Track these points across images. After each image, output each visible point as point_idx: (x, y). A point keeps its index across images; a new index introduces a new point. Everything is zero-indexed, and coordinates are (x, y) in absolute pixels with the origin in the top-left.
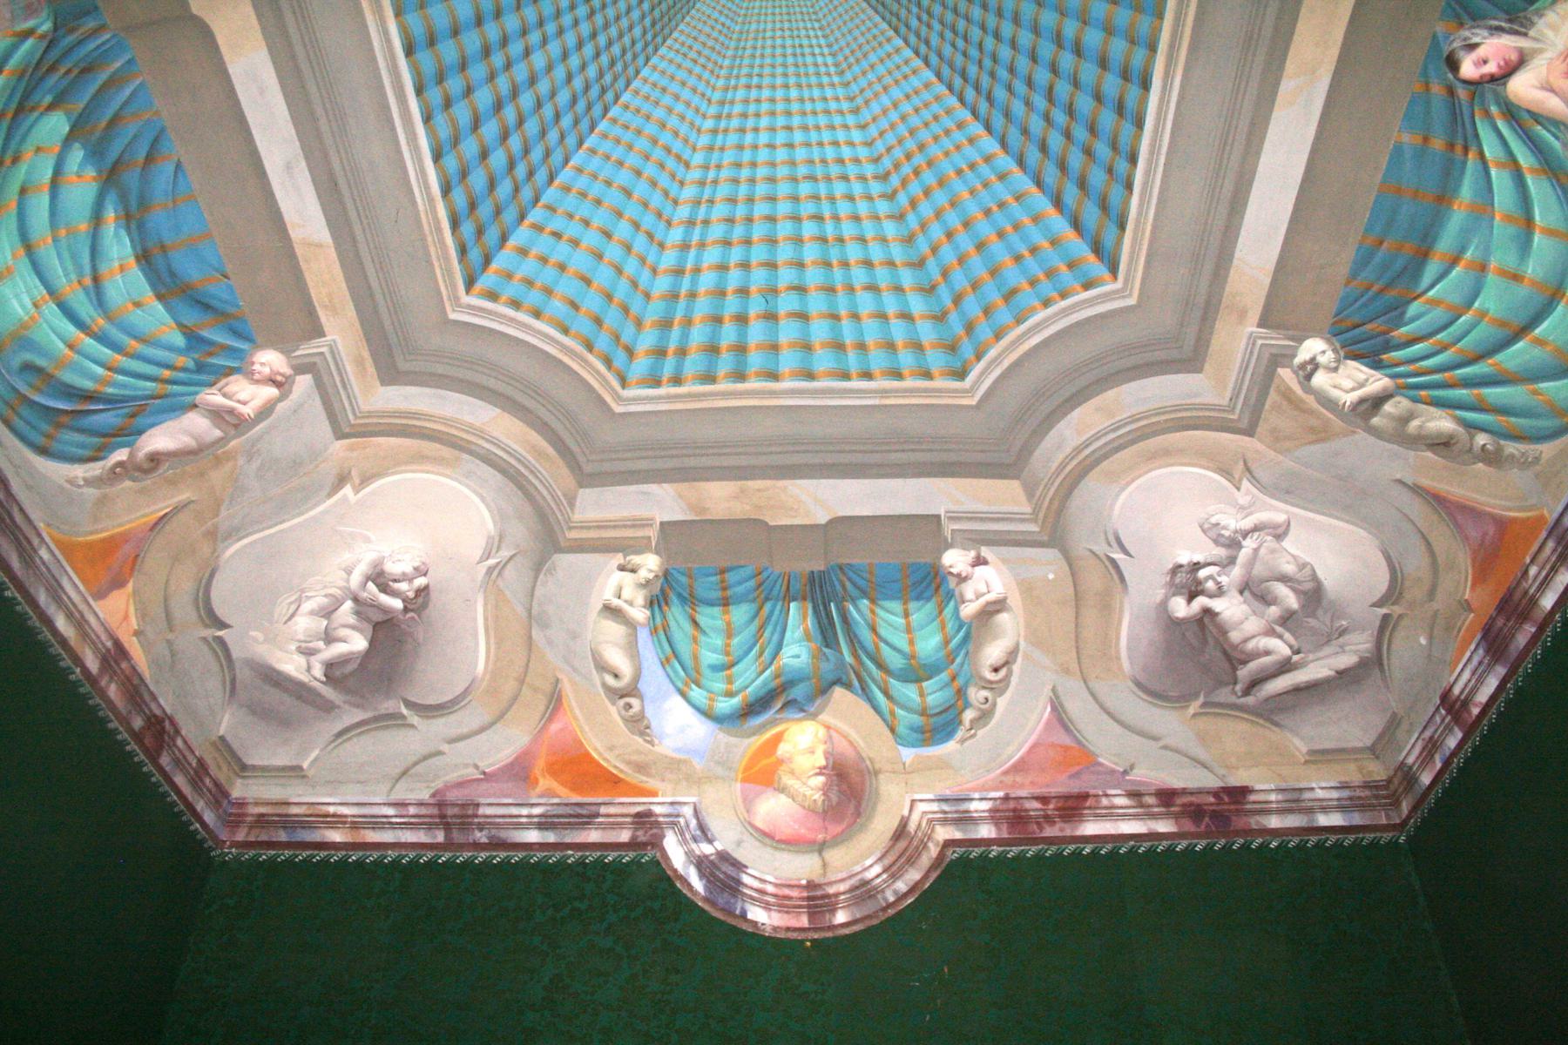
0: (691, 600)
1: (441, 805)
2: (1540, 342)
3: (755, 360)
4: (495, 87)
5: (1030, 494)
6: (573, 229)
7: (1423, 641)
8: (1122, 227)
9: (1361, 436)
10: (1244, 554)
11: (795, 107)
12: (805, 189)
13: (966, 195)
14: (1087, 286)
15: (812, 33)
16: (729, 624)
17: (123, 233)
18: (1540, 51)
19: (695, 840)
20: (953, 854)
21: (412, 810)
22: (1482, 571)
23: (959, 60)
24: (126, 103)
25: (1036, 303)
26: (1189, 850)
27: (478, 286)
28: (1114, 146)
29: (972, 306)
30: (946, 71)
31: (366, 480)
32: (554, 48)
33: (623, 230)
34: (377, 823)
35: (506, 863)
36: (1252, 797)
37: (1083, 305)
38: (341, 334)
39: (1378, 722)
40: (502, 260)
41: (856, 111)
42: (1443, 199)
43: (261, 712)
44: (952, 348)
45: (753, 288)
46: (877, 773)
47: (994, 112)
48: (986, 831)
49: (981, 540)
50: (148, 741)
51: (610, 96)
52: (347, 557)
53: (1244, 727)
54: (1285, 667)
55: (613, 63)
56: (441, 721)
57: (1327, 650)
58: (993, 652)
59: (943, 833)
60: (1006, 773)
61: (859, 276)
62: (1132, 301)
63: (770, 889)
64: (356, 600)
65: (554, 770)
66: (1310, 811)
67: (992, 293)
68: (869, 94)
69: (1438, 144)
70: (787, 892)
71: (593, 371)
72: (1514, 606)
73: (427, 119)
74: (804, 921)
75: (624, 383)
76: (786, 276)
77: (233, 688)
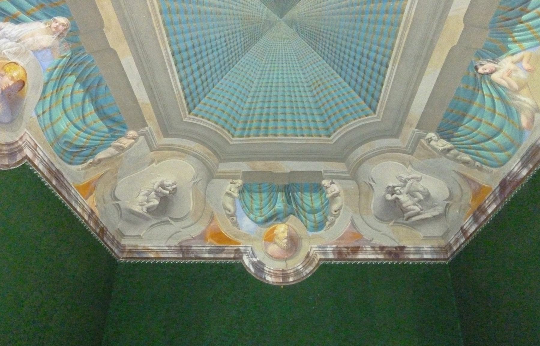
0: (250, 191)
1: (181, 246)
2: (495, 142)
3: (271, 131)
5: (347, 167)
7: (457, 211)
8: (378, 102)
9: (444, 159)
10: (408, 185)
13: (333, 92)
16: (261, 198)
17: (91, 104)
18: (501, 69)
19: (251, 257)
20: (322, 263)
21: (173, 248)
22: (474, 198)
24: (91, 72)
26: (387, 264)
27: (193, 112)
28: (377, 81)
30: (329, 61)
31: (158, 162)
32: (215, 54)
34: (163, 252)
35: (200, 263)
36: (406, 249)
37: (365, 120)
38: (152, 126)
39: (444, 230)
40: (199, 106)
42: (471, 102)
43: (129, 221)
44: (327, 129)
45: (271, 113)
46: (302, 239)
48: (331, 256)
49: (333, 178)
50: (101, 235)
51: (231, 65)
52: (153, 181)
53: (405, 229)
54: (418, 214)
55: (232, 57)
56: (180, 223)
57: (431, 210)
58: (335, 207)
59: (319, 257)
60: (338, 239)
62: (380, 120)
63: (272, 271)
64: (155, 191)
65: (212, 237)
66: (422, 254)
69: (471, 88)
70: (276, 272)
71: (225, 134)
72: (481, 210)
74: (281, 280)
75: (233, 136)
77: (121, 216)
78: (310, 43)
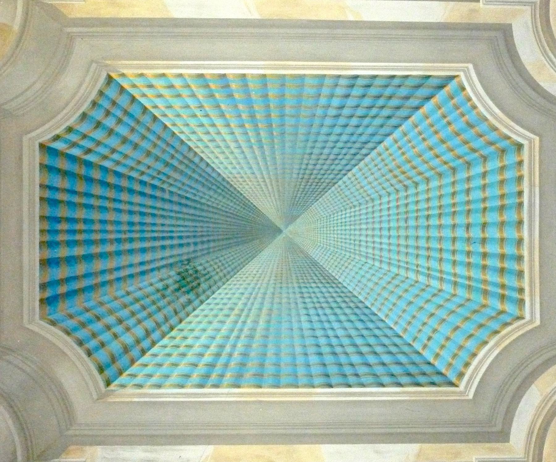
3: (509, 250)
4: (351, 353)
6: (427, 331)
8: (429, 77)
11: (370, 226)
12: (412, 223)
14: (463, 89)
15: (336, 218)
23: (348, 157)
25: (474, 112)
27: (454, 380)
29: (478, 143)
33: (430, 308)
37: (474, 88)
41: (373, 200)
47: (373, 140)
51: (360, 305)
55: (345, 302)
61: (461, 198)
62: (470, 66)
67: (469, 134)
68: (364, 194)
71: (511, 333)
73: (363, 385)
75: (520, 318)
76: (461, 233)
78: (325, 190)
